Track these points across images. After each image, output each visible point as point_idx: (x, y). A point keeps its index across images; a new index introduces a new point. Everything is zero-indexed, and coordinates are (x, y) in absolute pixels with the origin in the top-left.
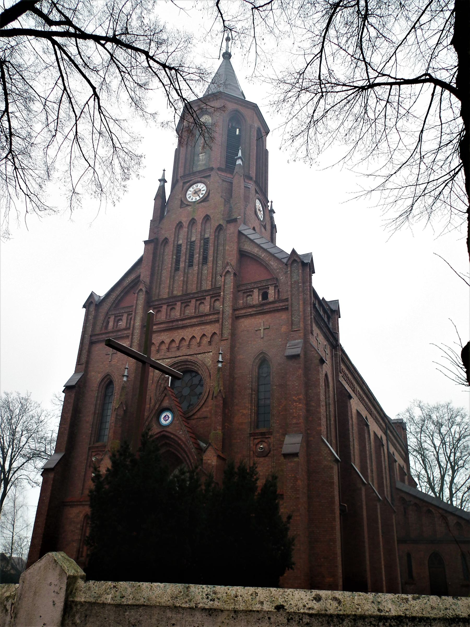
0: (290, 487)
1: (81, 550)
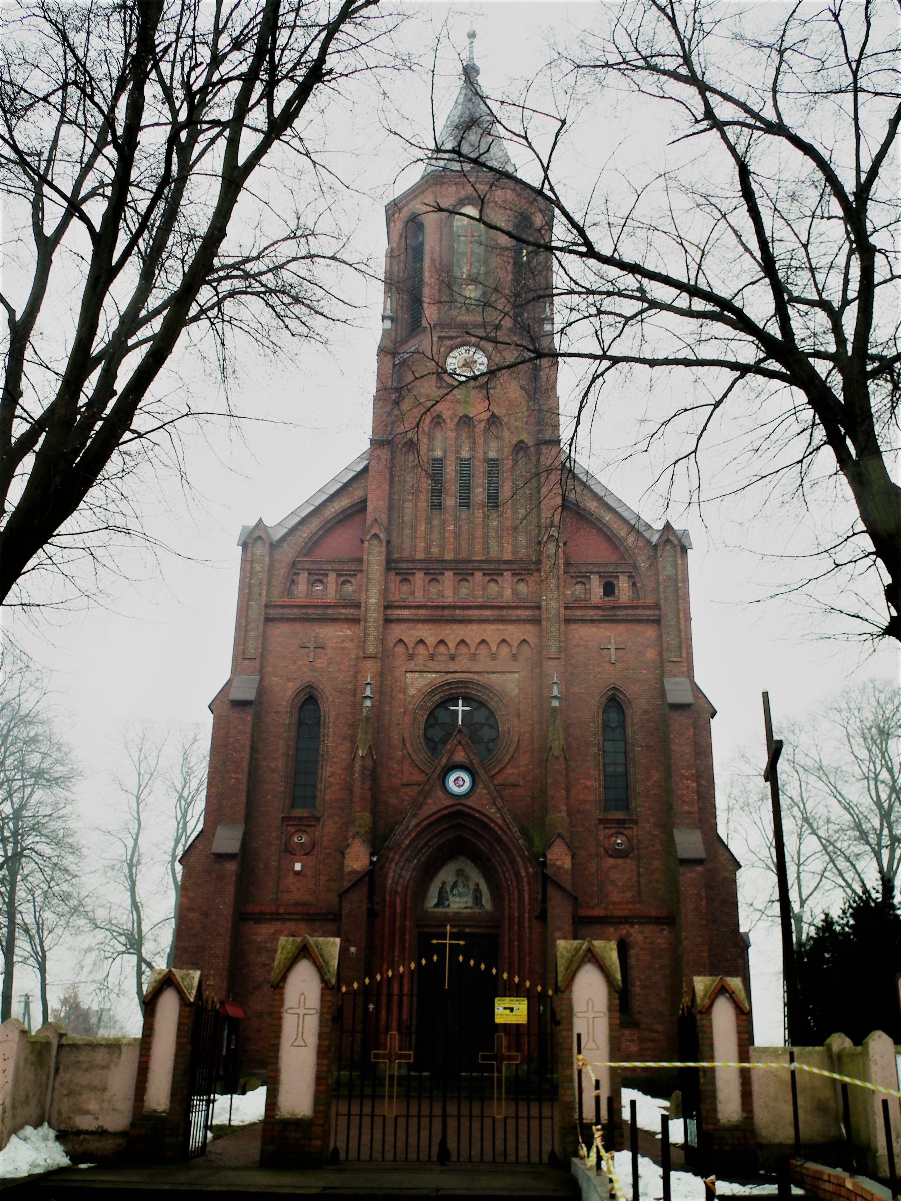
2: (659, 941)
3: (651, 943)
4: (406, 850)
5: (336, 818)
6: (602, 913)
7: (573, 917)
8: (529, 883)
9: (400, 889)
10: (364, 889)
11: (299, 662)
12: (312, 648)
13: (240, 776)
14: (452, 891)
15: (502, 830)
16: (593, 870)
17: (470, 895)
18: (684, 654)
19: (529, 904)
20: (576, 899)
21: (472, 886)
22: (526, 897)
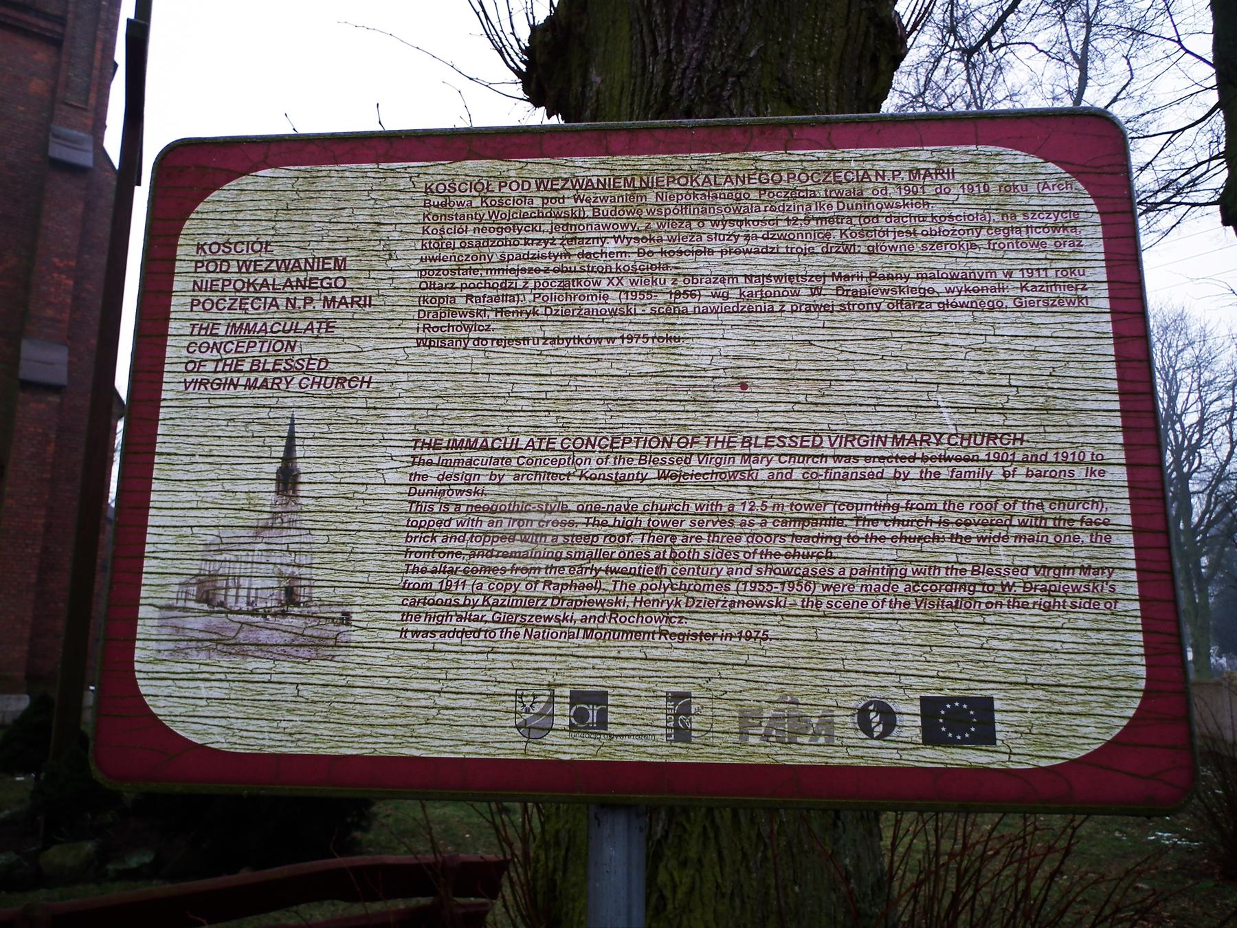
18: (92, 101)
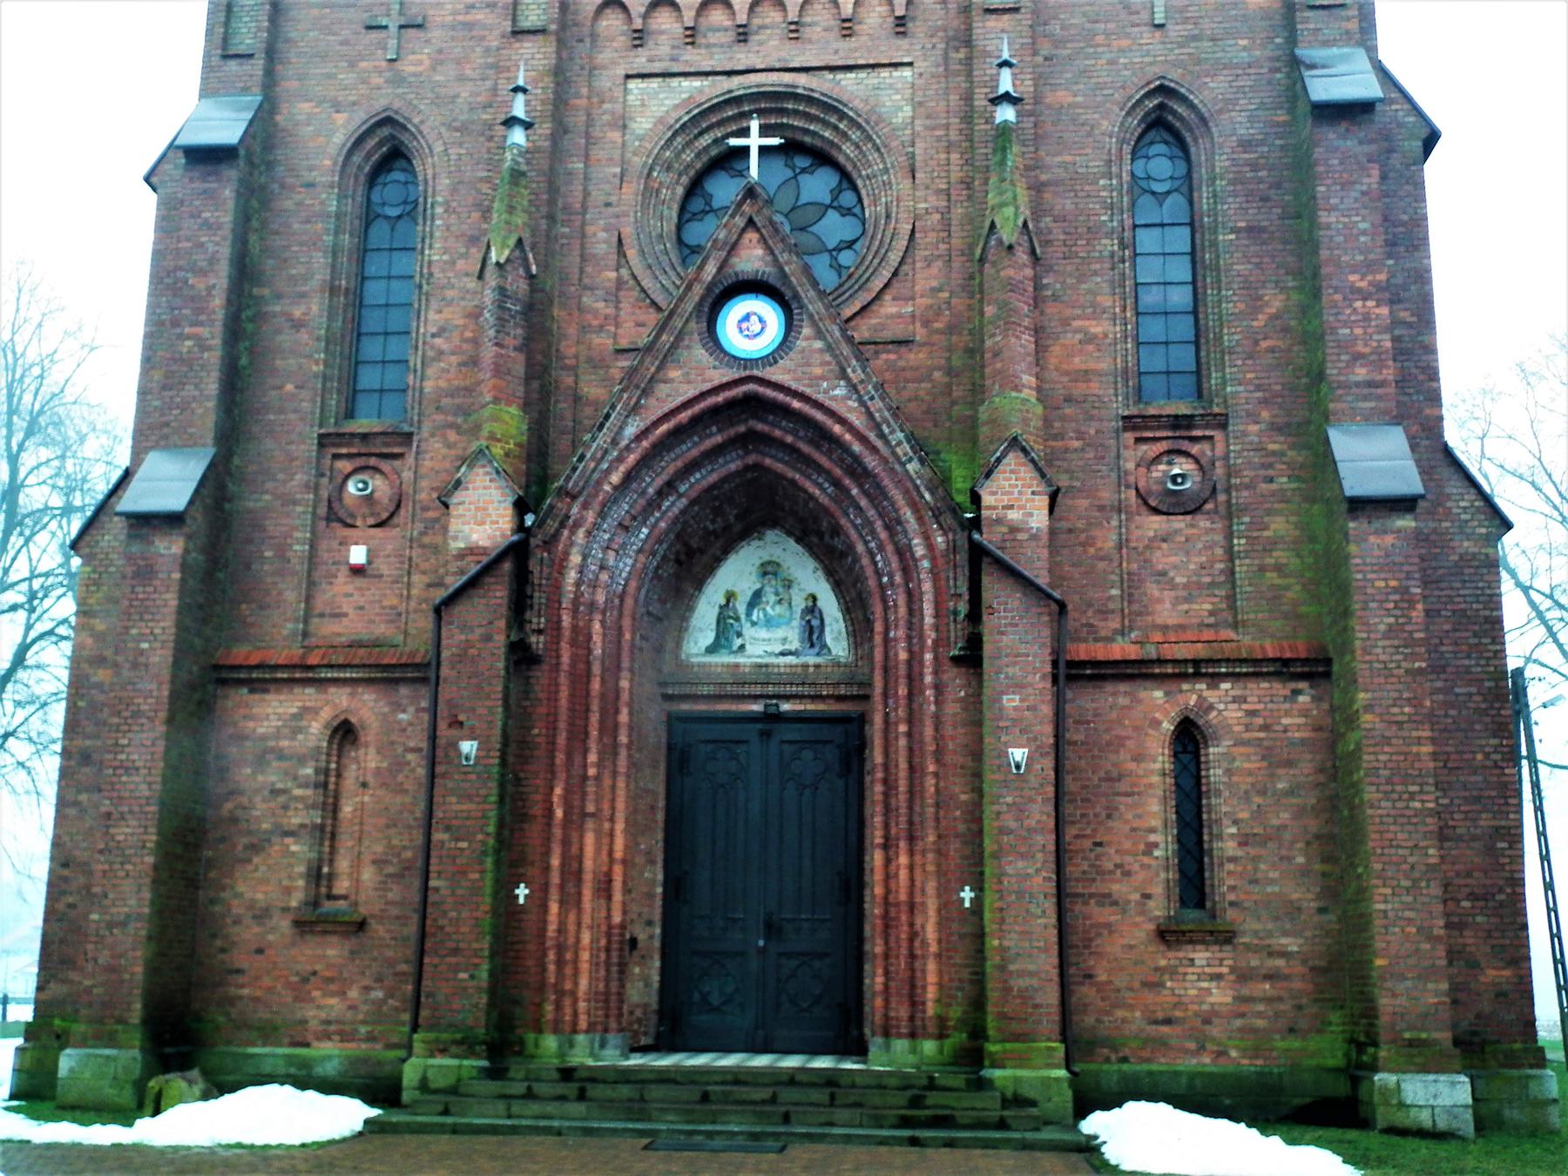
0: (1382, 627)
1: (325, 870)
2: (1285, 721)
3: (1265, 728)
4: (613, 500)
5: (452, 436)
6: (1133, 652)
7: (1055, 664)
8: (935, 573)
9: (601, 598)
10: (498, 594)
11: (363, 65)
12: (393, 29)
13: (204, 332)
14: (749, 614)
15: (863, 439)
16: (1111, 544)
17: (796, 623)
19: (937, 628)
20: (1062, 606)
21: (799, 603)
22: (928, 609)
